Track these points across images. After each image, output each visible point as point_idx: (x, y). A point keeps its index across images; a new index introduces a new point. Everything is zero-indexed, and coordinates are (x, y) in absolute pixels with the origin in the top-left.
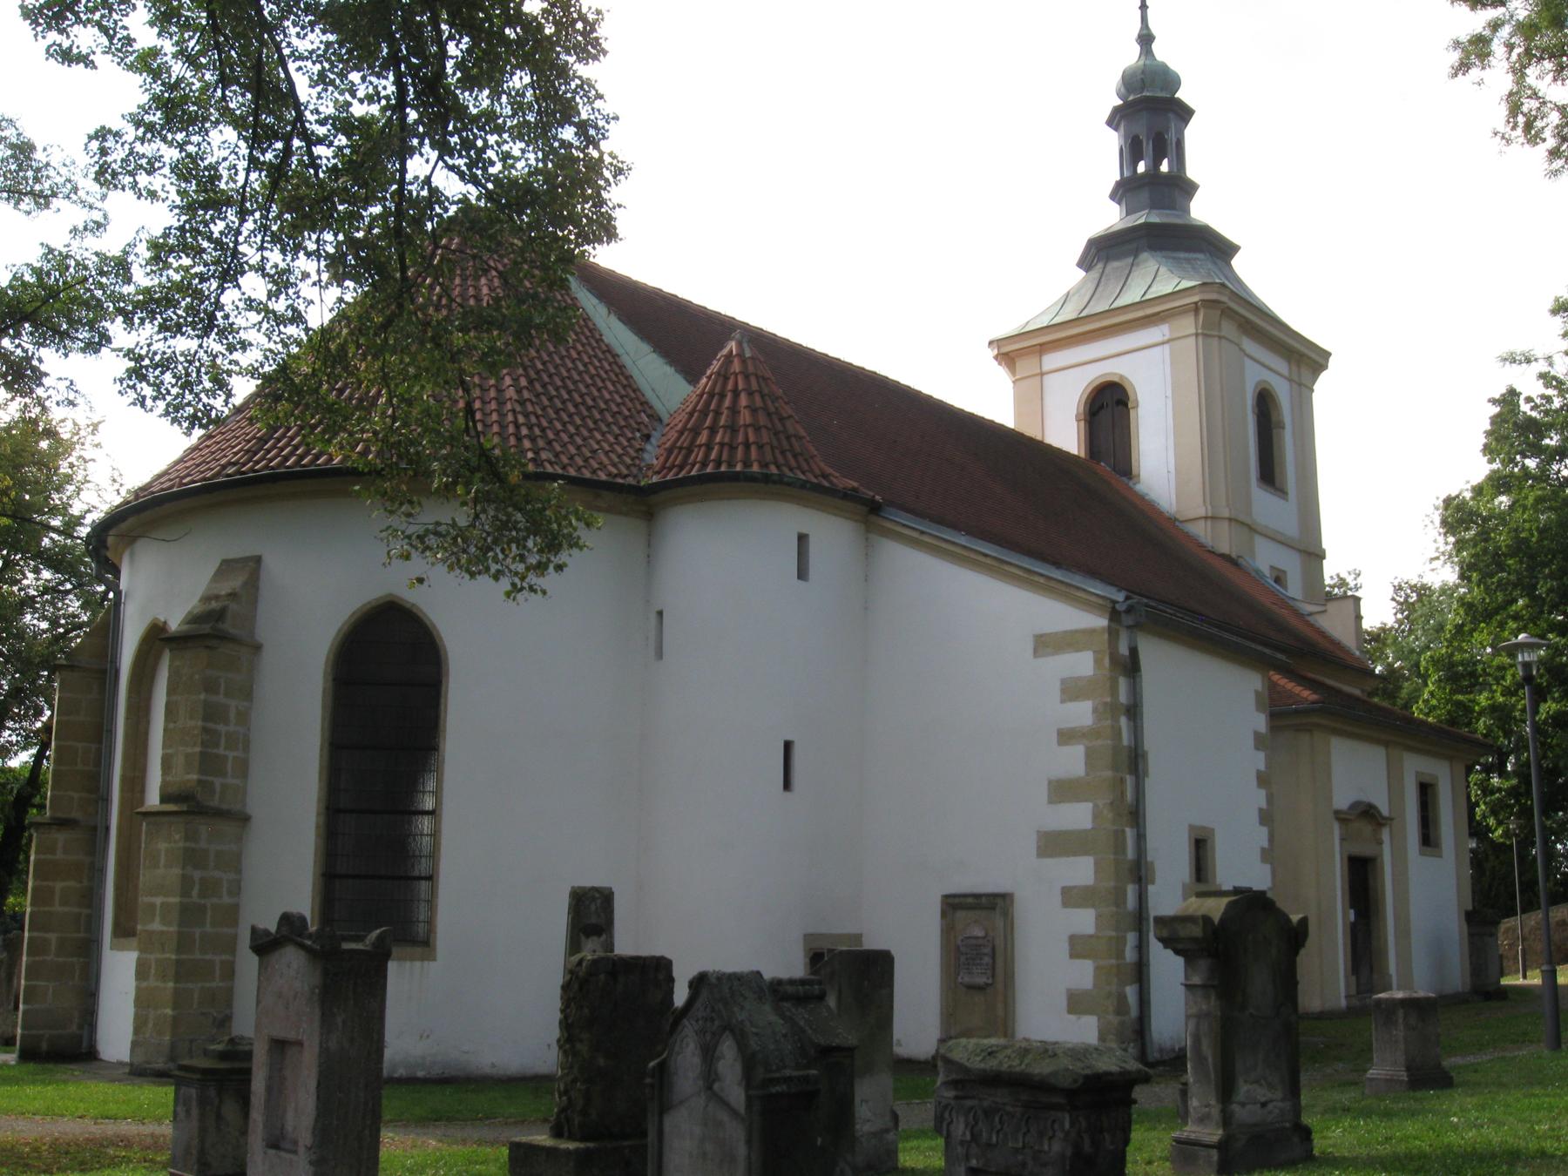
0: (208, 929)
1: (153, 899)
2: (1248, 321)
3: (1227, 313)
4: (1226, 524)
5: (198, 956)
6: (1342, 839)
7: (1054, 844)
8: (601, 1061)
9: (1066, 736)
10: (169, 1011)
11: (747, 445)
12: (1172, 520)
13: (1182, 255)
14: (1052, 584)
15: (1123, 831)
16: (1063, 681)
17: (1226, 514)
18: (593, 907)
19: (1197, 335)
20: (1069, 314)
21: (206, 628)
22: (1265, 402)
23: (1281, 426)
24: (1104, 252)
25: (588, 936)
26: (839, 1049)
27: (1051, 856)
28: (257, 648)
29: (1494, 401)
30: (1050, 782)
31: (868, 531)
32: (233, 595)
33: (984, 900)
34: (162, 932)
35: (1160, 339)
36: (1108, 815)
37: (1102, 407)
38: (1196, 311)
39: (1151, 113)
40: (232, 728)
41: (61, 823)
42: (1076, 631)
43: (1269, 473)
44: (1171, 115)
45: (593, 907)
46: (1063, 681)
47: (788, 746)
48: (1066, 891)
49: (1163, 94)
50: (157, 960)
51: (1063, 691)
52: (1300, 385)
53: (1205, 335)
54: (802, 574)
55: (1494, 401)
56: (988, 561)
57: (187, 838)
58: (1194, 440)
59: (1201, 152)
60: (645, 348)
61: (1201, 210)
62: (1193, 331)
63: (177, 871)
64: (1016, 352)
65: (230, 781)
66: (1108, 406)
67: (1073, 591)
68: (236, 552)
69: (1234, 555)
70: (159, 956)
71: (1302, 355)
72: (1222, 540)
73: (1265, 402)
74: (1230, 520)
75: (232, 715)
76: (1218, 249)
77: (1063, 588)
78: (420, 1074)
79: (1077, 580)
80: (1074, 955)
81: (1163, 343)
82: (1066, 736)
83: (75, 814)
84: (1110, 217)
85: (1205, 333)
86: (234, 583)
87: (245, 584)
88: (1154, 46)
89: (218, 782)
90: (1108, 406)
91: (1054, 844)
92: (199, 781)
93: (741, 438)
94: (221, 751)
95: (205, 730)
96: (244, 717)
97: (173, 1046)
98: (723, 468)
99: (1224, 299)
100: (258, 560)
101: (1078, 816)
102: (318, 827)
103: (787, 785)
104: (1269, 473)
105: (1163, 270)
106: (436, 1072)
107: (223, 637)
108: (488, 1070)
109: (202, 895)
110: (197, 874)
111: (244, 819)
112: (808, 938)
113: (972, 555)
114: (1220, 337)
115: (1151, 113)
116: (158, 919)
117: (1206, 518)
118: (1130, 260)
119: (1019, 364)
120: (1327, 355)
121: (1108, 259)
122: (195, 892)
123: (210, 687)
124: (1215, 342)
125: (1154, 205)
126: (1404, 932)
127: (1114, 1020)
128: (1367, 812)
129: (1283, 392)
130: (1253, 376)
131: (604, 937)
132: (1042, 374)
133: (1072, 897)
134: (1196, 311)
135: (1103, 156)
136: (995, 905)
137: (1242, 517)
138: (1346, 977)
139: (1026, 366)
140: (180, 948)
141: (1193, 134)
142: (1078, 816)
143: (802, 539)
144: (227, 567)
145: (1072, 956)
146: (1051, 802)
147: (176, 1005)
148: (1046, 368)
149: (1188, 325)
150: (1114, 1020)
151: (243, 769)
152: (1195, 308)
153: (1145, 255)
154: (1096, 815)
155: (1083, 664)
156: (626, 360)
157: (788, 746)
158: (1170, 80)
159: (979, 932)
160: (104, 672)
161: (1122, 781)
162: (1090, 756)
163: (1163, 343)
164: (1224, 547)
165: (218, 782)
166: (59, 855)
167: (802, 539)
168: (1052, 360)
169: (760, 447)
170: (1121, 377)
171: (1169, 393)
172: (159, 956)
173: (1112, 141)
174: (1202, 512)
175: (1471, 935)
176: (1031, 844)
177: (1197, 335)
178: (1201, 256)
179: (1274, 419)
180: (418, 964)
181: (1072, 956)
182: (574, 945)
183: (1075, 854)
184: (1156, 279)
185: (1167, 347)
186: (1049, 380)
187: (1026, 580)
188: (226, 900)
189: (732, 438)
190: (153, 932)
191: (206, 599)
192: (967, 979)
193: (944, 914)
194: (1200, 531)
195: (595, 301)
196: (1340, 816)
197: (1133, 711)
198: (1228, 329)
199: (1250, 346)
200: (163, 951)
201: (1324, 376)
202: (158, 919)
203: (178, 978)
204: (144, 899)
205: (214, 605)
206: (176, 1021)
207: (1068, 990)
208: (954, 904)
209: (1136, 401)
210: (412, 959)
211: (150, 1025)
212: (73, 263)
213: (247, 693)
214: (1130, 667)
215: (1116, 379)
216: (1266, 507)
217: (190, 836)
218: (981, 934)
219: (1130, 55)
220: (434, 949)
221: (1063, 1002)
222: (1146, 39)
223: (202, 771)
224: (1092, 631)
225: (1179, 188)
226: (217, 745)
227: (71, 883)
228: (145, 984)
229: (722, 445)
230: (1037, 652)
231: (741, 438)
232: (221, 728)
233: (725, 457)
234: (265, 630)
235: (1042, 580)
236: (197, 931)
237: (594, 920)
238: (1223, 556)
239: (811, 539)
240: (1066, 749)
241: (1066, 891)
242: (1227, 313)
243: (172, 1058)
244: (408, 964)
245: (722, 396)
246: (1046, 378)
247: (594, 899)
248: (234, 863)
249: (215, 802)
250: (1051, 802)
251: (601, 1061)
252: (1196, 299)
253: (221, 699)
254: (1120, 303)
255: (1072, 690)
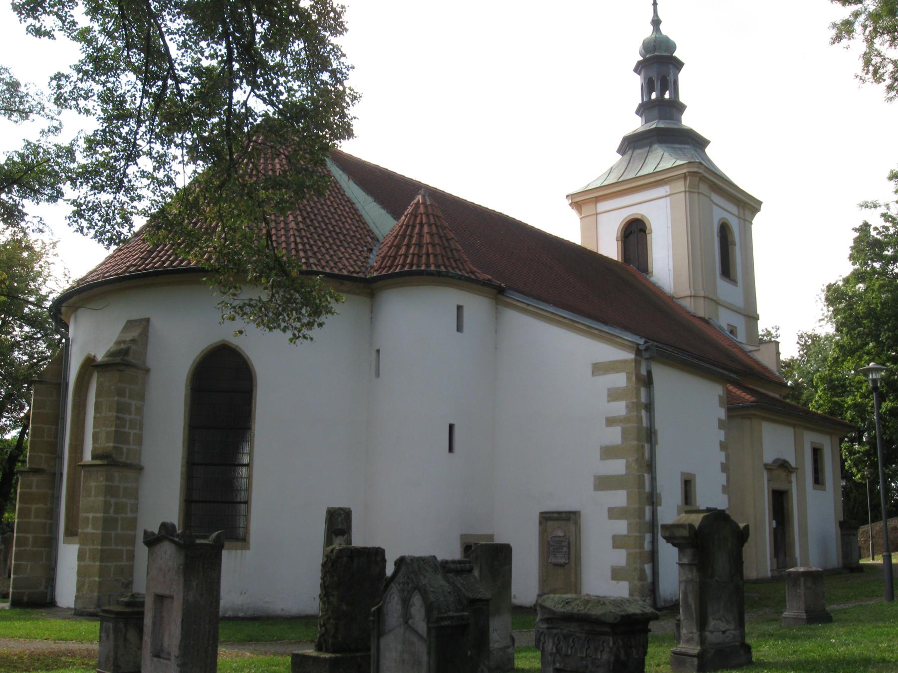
0: (119, 531)
1: (87, 515)
2: (715, 184)
3: (703, 179)
4: (702, 300)
5: (113, 547)
6: (769, 480)
7: (604, 483)
8: (344, 607)
9: (611, 421)
10: (97, 579)
11: (428, 255)
12: (671, 298)
13: (677, 146)
14: (602, 334)
15: (643, 476)
16: (609, 390)
17: (702, 294)
18: (340, 519)
19: (685, 192)
20: (612, 179)
21: (118, 360)
22: (724, 230)
23: (734, 244)
24: (632, 144)
25: (337, 536)
26: (480, 600)
27: (602, 490)
28: (147, 371)
29: (855, 230)
30: (601, 448)
31: (497, 304)
32: (133, 341)
33: (563, 515)
34: (93, 534)
35: (664, 194)
36: (635, 466)
37: (631, 233)
38: (685, 178)
39: (659, 65)
40: (133, 417)
41: (35, 471)
42: (616, 361)
43: (727, 271)
44: (671, 66)
45: (340, 519)
46: (609, 390)
47: (451, 427)
48: (610, 510)
49: (666, 54)
50: (90, 550)
51: (609, 395)
52: (745, 220)
53: (690, 192)
54: (459, 328)
55: (855, 230)
56: (566, 321)
57: (107, 480)
58: (684, 252)
59: (688, 87)
60: (369, 199)
61: (688, 120)
62: (683, 189)
63: (101, 498)
64: (582, 201)
65: (132, 447)
66: (635, 233)
67: (614, 338)
68: (135, 316)
69: (707, 318)
70: (91, 547)
71: (746, 203)
72: (700, 309)
73: (724, 230)
74: (704, 297)
75: (133, 409)
76: (697, 142)
77: (609, 337)
78: (241, 615)
79: (617, 332)
80: (615, 546)
81: (666, 196)
82: (611, 421)
83: (43, 466)
84: (636, 124)
85: (690, 191)
86: (134, 334)
87: (141, 334)
88: (661, 26)
89: (125, 447)
90: (635, 233)
91: (604, 483)
92: (114, 447)
93: (424, 251)
94: (127, 430)
95: (118, 418)
96: (140, 411)
97: (99, 599)
98: (414, 268)
99: (701, 171)
100: (148, 320)
101: (618, 467)
102: (182, 473)
103: (451, 449)
104: (727, 271)
105: (666, 154)
106: (250, 613)
107: (128, 365)
108: (279, 613)
109: (116, 512)
110: (113, 500)
111: (140, 469)
112: (463, 537)
113: (557, 318)
114: (699, 193)
115: (659, 65)
116: (90, 526)
117: (691, 296)
118: (647, 149)
119: (584, 208)
120: (760, 203)
121: (634, 148)
122: (112, 511)
123: (120, 393)
124: (696, 196)
125: (661, 117)
126: (804, 534)
127: (638, 583)
128: (783, 465)
129: (735, 224)
130: (718, 215)
131: (346, 536)
132: (597, 214)
133: (614, 513)
134: (685, 178)
135: (632, 89)
136: (570, 518)
137: (711, 296)
138: (771, 559)
139: (588, 209)
140: (103, 543)
141: (683, 77)
142: (618, 467)
143: (460, 308)
144: (130, 325)
145: (614, 547)
146: (602, 459)
147: (101, 575)
148: (599, 211)
149: (680, 186)
150: (638, 583)
151: (139, 440)
152: (685, 176)
153: (655, 146)
154: (628, 467)
155: (620, 380)
156: (358, 206)
157: (451, 427)
158: (670, 46)
159: (560, 534)
160: (60, 384)
161: (643, 447)
162: (624, 432)
163: (666, 196)
164: (701, 313)
165: (125, 447)
166: (34, 490)
167: (460, 308)
168: (602, 206)
169: (435, 256)
170: (642, 216)
171: (670, 225)
172: (91, 547)
173: (637, 81)
174: (688, 293)
175: (842, 535)
176: (591, 483)
177: (685, 192)
178: (688, 146)
179: (730, 240)
180: (239, 552)
181: (614, 547)
182: (329, 541)
183: (616, 489)
184: (662, 160)
185: (668, 198)
186: (601, 218)
187: (588, 332)
188: (130, 515)
189: (419, 251)
190: (88, 533)
191: (118, 343)
192: (554, 561)
193: (540, 523)
194: (688, 304)
195: (341, 172)
196: (767, 467)
197: (649, 407)
198: (704, 188)
199: (716, 198)
200: (94, 544)
201: (758, 215)
202: (90, 526)
203: (102, 560)
204: (82, 515)
205: (123, 346)
206: (101, 585)
207: (612, 567)
208: (546, 518)
209: (651, 229)
210: (236, 549)
211: (86, 587)
212: (42, 151)
213: (142, 397)
214: (647, 382)
215: (639, 217)
216: (725, 290)
217: (109, 478)
218: (562, 534)
219: (647, 32)
220: (249, 543)
221: (609, 574)
222: (656, 22)
223: (116, 441)
224: (625, 361)
225: (675, 108)
226: (124, 426)
227: (41, 506)
228: (83, 563)
229: (413, 254)
230: (594, 373)
231: (424, 251)
232: (127, 417)
233: (415, 261)
234: (152, 361)
235: (597, 332)
236: (113, 533)
237: (340, 527)
238: (700, 318)
239: (465, 309)
240: (610, 429)
241: (610, 510)
242: (703, 179)
243: (99, 605)
244: (234, 552)
245: (414, 227)
246: (599, 216)
247: (340, 514)
248: (134, 494)
249: (123, 459)
250: (602, 459)
251: (344, 607)
252: (685, 171)
253: (126, 400)
254: (641, 173)
255: (614, 395)
